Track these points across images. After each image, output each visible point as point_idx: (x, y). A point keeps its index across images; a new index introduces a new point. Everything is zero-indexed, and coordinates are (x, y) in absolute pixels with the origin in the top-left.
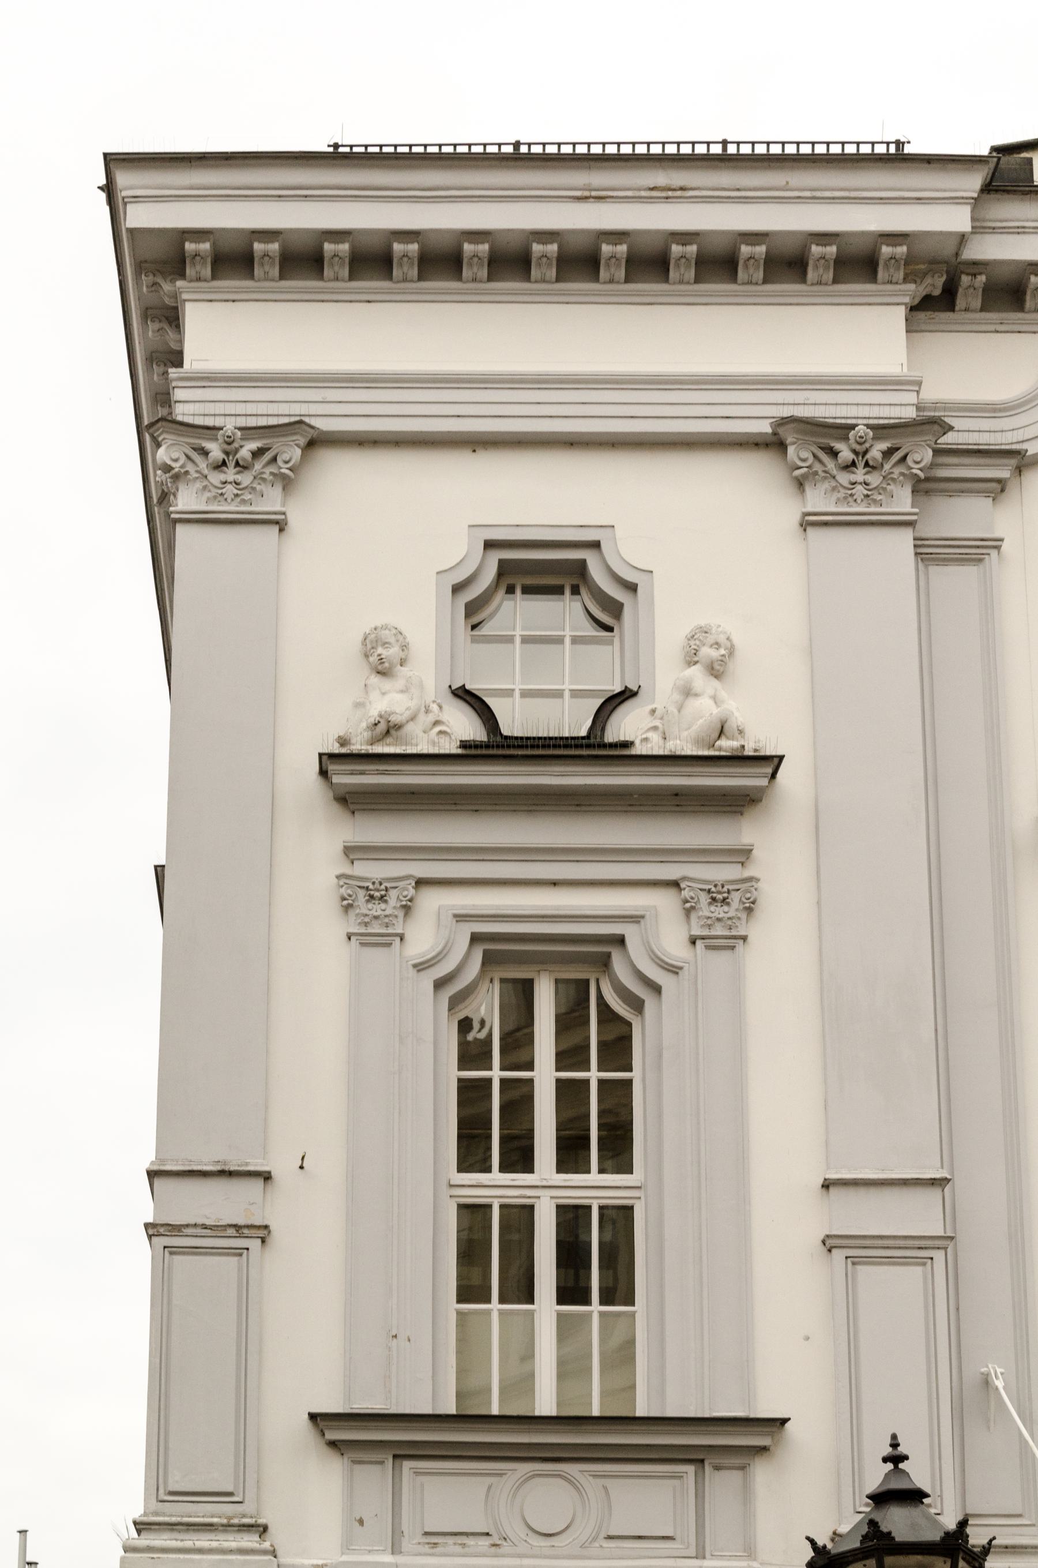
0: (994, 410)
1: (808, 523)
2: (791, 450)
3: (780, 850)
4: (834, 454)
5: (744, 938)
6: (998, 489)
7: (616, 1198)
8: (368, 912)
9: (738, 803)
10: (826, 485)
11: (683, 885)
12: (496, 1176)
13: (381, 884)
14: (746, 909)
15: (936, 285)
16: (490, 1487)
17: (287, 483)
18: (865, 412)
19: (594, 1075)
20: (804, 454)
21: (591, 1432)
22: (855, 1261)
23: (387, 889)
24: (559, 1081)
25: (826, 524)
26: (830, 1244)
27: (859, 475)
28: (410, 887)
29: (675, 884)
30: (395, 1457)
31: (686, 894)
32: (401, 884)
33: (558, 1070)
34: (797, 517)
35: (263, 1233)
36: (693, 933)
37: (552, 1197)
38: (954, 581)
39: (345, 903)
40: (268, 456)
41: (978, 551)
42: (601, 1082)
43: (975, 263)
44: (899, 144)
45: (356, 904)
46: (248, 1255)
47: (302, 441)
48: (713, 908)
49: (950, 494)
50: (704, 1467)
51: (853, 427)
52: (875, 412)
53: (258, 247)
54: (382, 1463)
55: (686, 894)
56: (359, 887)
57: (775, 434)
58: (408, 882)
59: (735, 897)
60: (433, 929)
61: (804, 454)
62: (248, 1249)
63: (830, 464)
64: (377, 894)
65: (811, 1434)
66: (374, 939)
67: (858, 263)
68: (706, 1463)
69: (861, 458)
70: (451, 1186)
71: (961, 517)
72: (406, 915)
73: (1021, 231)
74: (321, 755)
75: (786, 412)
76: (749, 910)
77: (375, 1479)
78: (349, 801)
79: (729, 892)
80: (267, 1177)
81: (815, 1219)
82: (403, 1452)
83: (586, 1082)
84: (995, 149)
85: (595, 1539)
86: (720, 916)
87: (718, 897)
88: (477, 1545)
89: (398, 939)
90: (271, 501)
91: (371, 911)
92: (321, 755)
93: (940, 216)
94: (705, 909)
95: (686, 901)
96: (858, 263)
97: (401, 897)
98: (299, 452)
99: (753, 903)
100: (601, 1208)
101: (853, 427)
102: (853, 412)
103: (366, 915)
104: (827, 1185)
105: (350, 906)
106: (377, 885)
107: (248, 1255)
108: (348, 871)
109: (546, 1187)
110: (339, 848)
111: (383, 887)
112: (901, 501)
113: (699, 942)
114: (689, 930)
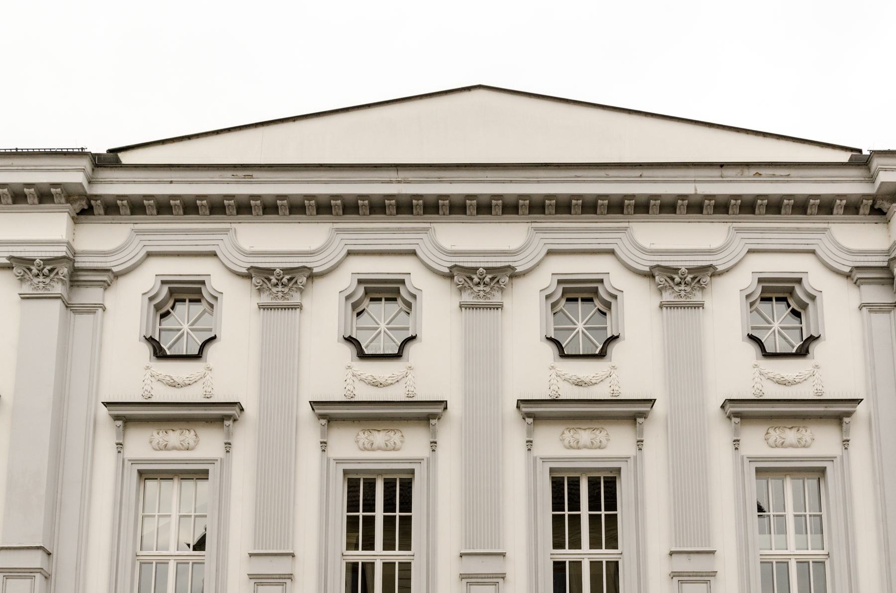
0: (104, 254)
1: (25, 297)
2: (657, 278)
4: (472, 279)
6: (106, 286)
7: (612, 558)
10: (469, 291)
12: (360, 552)
15: (83, 204)
17: (301, 291)
18: (40, 254)
19: (361, 514)
20: (662, 279)
24: (590, 515)
25: (28, 298)
26: (463, 577)
27: (682, 287)
33: (385, 512)
34: (658, 304)
35: (290, 577)
38: (83, 321)
40: (294, 281)
41: (91, 309)
42: (606, 515)
43: (96, 196)
44: (82, 149)
47: (307, 274)
49: (87, 286)
51: (35, 260)
52: (44, 254)
53: (414, 202)
57: (651, 271)
61: (662, 279)
63: (672, 284)
67: (45, 196)
69: (683, 282)
71: (89, 296)
73: (111, 182)
75: (655, 264)
80: (503, 555)
83: (395, 516)
84: (110, 151)
90: (295, 299)
93: (74, 176)
96: (45, 196)
98: (305, 279)
100: (607, 562)
101: (35, 260)
102: (36, 254)
109: (379, 556)
112: (58, 289)
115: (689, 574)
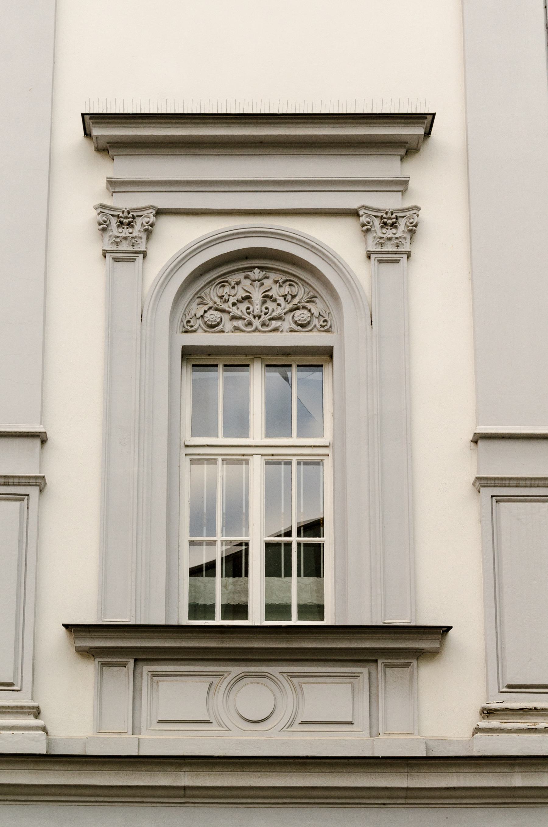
3: (435, 188)
5: (408, 255)
8: (119, 235)
9: (408, 149)
11: (361, 213)
13: (129, 213)
14: (146, 230)
16: (211, 685)
21: (413, 639)
22: (498, 499)
23: (397, 218)
28: (151, 215)
29: (354, 213)
30: (136, 660)
31: (363, 219)
32: (145, 213)
35: (39, 482)
36: (368, 250)
37: (262, 455)
39: (365, 228)
45: (373, 229)
46: (28, 499)
48: (384, 231)
50: (377, 665)
54: (124, 665)
55: (363, 219)
56: (112, 215)
58: (151, 211)
59: (402, 223)
60: (178, 241)
62: (28, 495)
64: (126, 220)
65: (469, 635)
66: (117, 256)
68: (380, 662)
70: (187, 446)
72: (148, 238)
74: (83, 115)
76: (412, 232)
77: (121, 678)
78: (107, 149)
79: (397, 218)
80: (41, 438)
81: (467, 467)
82: (142, 656)
85: (291, 726)
86: (389, 236)
87: (389, 221)
88: (531, 726)
89: (405, 256)
91: (124, 233)
92: (83, 115)
94: (114, 230)
95: (363, 225)
97: (408, 224)
99: (416, 226)
103: (118, 237)
104: (475, 442)
105: (368, 230)
106: (389, 215)
107: (28, 499)
108: (108, 202)
110: (103, 183)
111: (130, 215)
113: (373, 256)
114: (366, 248)
115: (518, 482)
